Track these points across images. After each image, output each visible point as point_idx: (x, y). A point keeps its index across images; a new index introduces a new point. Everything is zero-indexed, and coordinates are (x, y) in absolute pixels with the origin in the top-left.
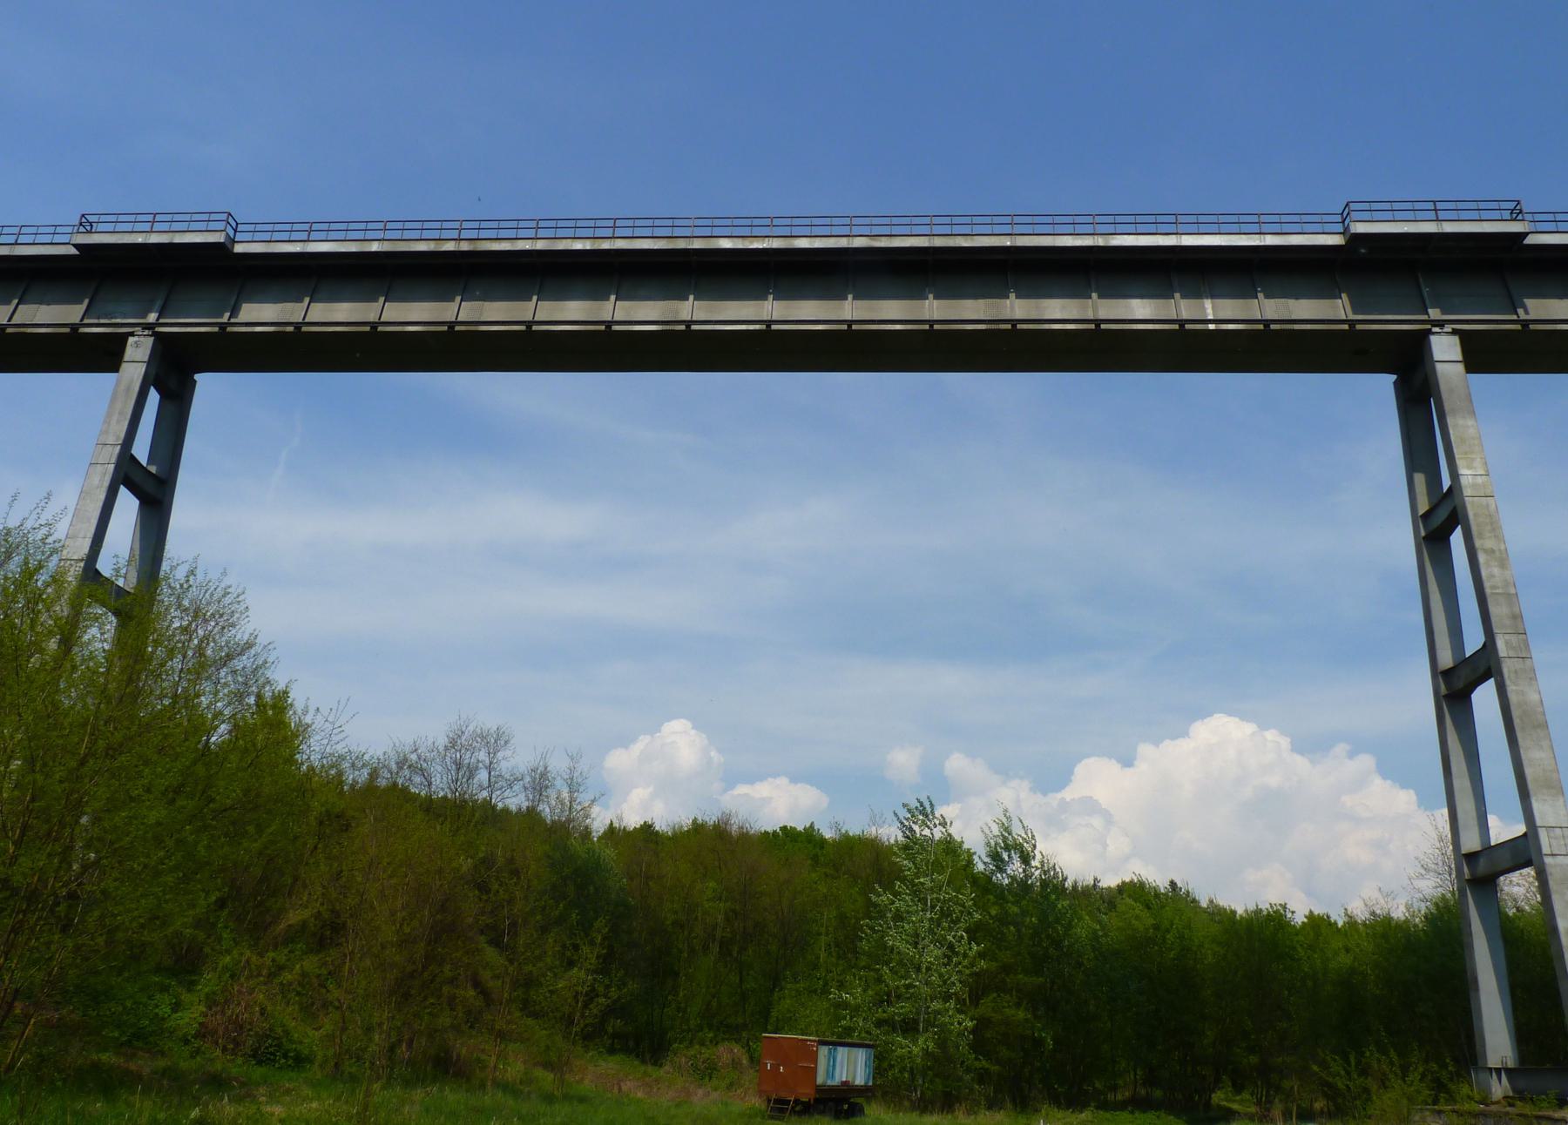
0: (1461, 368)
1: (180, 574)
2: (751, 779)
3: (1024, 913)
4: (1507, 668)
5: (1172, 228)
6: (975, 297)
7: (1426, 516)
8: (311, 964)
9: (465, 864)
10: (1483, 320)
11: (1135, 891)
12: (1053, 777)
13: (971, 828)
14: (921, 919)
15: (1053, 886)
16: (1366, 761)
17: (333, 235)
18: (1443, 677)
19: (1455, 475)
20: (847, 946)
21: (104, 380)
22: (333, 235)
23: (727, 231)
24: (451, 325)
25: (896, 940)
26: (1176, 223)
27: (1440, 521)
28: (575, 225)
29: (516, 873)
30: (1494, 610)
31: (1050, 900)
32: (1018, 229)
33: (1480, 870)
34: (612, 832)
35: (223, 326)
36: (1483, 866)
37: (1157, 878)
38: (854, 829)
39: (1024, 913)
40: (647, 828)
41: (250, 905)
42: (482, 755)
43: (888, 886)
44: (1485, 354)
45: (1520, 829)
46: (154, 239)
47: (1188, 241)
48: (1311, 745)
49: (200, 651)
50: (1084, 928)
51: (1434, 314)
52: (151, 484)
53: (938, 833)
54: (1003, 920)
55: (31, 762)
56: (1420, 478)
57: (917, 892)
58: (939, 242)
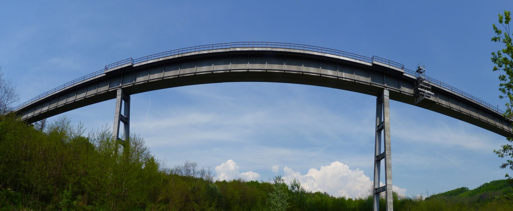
0: (388, 98)
1: (133, 137)
2: (245, 171)
3: (297, 197)
4: (387, 157)
5: (338, 54)
6: (295, 65)
7: (378, 126)
8: (164, 206)
9: (190, 189)
10: (394, 89)
11: (318, 194)
12: (304, 172)
13: (288, 181)
14: (278, 198)
15: (303, 192)
16: (362, 172)
17: (152, 58)
18: (377, 157)
19: (384, 119)
20: (263, 203)
21: (114, 100)
22: (152, 58)
23: (238, 46)
24: (179, 75)
25: (273, 202)
26: (339, 53)
27: (380, 128)
28: (204, 47)
29: (200, 190)
30: (387, 146)
31: (302, 194)
32: (305, 49)
33: (377, 191)
34: (217, 182)
35: (134, 84)
36: (378, 191)
37: (322, 191)
38: (265, 181)
39: (297, 197)
40: (224, 181)
41: (153, 197)
42: (192, 168)
43: (272, 192)
44: (394, 96)
45: (385, 185)
46: (119, 68)
47: (341, 58)
48: (353, 168)
49: (138, 151)
50: (308, 200)
51: (386, 85)
52: (125, 120)
53: (282, 182)
54: (293, 199)
55: (114, 173)
56: (378, 119)
57: (277, 193)
58: (287, 50)
